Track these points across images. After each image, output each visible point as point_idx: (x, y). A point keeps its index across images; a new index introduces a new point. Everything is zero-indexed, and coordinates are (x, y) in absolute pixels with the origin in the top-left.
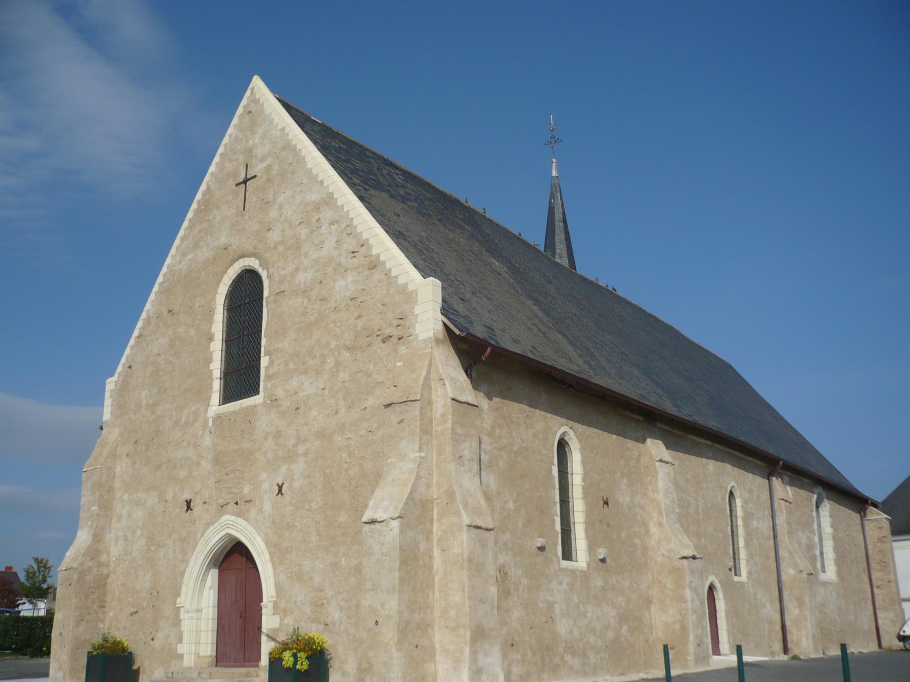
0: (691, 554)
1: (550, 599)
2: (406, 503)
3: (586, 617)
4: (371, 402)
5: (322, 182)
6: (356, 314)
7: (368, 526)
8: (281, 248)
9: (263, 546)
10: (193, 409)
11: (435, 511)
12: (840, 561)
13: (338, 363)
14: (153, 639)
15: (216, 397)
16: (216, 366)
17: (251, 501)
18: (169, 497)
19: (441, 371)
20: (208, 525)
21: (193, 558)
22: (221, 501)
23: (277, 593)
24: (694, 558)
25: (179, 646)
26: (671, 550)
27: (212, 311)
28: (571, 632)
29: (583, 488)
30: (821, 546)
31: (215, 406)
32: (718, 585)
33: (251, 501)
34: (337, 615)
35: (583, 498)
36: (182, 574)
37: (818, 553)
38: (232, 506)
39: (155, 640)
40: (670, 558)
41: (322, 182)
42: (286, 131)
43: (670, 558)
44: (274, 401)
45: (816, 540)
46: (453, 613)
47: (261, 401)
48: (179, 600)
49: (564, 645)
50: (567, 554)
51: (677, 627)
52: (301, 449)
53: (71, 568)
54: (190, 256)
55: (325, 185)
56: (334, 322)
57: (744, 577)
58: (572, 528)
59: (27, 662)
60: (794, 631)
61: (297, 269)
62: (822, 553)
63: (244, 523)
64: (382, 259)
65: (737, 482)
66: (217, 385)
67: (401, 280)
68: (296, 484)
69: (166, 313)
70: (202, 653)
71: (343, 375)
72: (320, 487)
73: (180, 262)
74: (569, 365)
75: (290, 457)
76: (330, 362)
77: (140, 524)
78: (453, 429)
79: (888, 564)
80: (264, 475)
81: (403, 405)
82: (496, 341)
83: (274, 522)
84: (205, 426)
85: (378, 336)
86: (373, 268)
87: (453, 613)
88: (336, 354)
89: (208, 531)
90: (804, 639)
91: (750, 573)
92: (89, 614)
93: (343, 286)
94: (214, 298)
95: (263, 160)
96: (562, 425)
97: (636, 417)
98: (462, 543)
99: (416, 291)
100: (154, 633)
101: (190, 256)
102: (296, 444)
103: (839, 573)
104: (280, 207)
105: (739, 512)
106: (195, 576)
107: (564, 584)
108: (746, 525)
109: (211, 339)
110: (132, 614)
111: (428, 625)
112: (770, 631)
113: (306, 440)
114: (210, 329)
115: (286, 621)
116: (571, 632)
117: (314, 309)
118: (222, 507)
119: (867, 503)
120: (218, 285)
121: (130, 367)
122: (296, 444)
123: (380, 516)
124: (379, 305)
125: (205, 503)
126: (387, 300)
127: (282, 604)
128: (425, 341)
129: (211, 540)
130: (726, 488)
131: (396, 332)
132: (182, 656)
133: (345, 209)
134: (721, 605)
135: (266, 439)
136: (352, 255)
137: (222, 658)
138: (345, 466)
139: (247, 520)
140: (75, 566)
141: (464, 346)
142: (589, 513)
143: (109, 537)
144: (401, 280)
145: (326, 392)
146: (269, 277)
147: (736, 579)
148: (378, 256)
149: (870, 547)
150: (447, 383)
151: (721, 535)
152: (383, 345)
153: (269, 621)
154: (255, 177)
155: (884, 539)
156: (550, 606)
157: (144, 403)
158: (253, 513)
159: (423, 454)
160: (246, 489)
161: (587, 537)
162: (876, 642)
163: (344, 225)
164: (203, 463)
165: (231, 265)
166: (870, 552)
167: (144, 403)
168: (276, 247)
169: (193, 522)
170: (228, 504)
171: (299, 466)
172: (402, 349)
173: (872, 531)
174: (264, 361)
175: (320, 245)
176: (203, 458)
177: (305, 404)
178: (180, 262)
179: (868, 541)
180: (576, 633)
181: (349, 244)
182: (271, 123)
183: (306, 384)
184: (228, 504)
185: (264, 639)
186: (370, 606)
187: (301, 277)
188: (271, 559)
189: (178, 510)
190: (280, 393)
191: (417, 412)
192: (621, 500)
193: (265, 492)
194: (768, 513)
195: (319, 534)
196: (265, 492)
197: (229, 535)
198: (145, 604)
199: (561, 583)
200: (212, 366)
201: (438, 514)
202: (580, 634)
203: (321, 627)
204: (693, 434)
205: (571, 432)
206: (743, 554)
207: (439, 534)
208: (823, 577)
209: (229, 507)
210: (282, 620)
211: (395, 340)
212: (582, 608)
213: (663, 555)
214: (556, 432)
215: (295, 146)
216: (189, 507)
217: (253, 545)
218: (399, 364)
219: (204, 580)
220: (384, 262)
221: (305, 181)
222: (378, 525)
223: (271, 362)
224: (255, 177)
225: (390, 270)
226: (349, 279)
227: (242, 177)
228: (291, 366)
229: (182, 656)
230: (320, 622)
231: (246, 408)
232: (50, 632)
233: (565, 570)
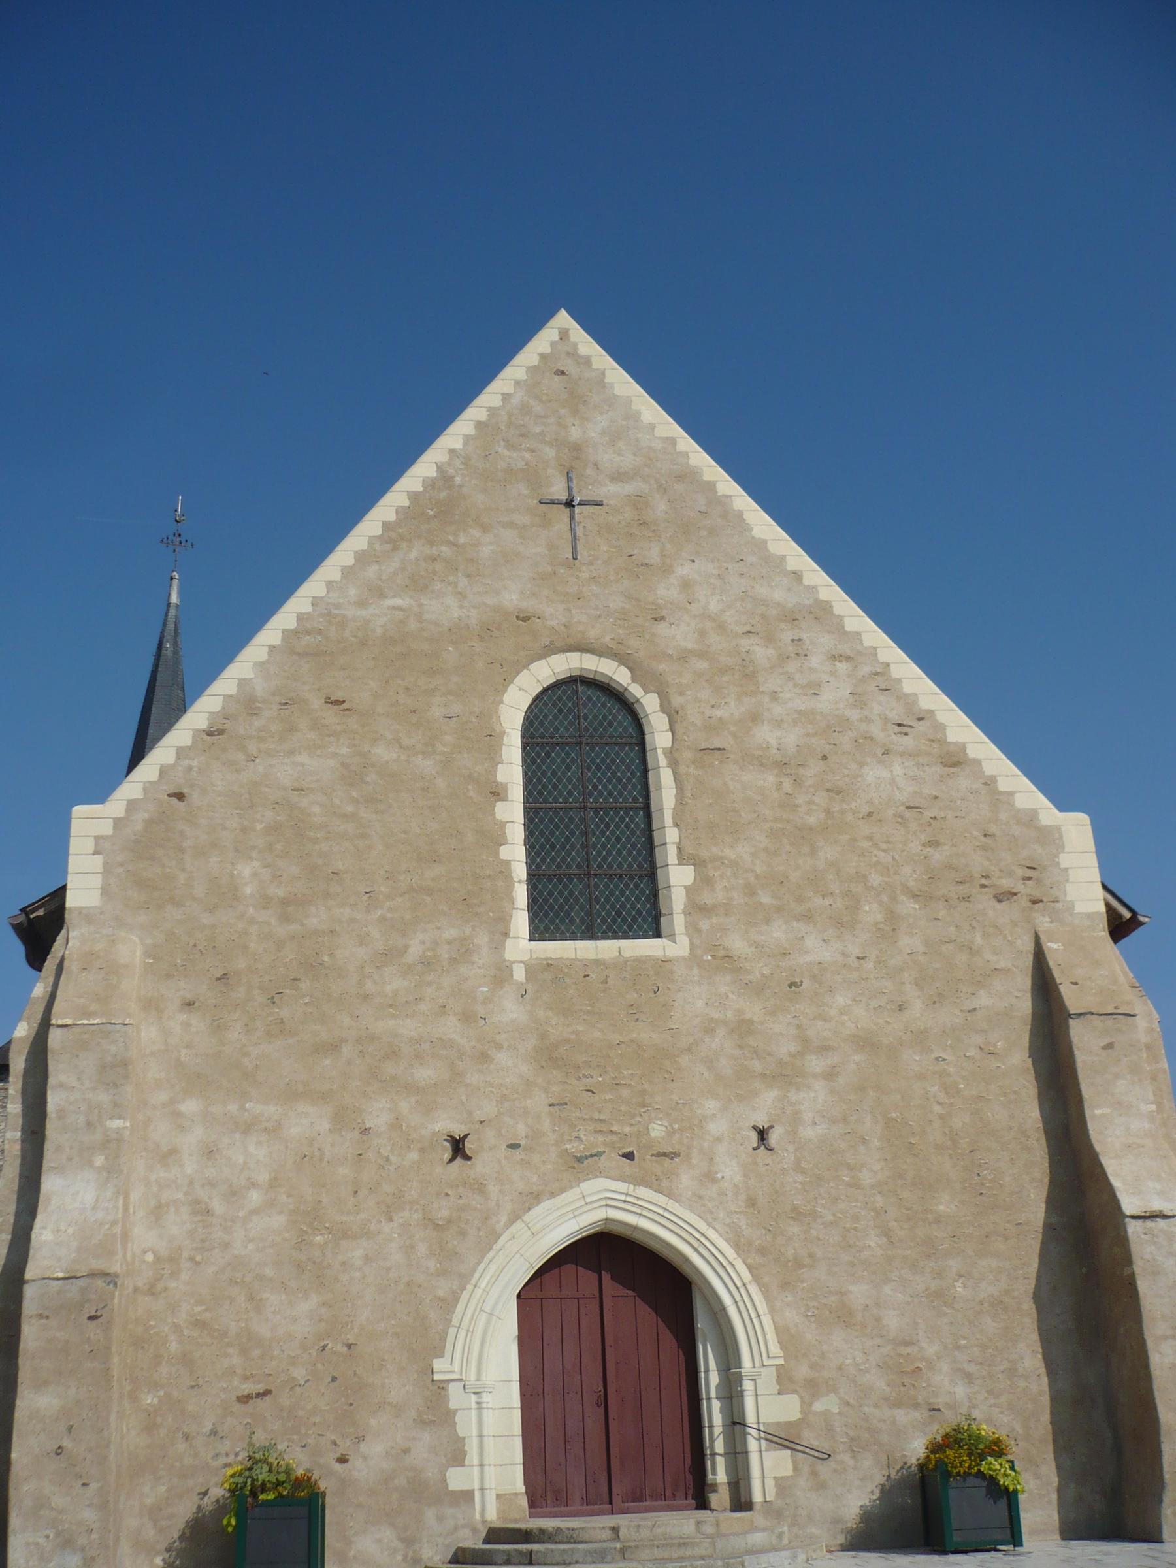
4: (983, 1000)
7: (1139, 1223)
10: (450, 933)
13: (892, 916)
15: (521, 921)
31: (520, 945)
38: (612, 1160)
39: (356, 1463)
61: (755, 718)
69: (317, 703)
71: (908, 942)
72: (876, 1143)
76: (871, 912)
77: (263, 1177)
81: (1109, 1022)
83: (752, 1202)
86: (955, 764)
88: (885, 898)
89: (537, 1211)
102: (801, 1054)
110: (245, 1399)
115: (818, 1406)
117: (811, 803)
118: (580, 1160)
120: (506, 687)
122: (801, 1054)
125: (514, 1146)
126: (993, 829)
136: (898, 729)
139: (670, 1195)
145: (869, 965)
146: (666, 708)
158: (686, 1180)
163: (866, 670)
164: (502, 1058)
169: (480, 1187)
170: (598, 1155)
171: (813, 1099)
175: (813, 689)
177: (814, 978)
178: (361, 604)
183: (810, 942)
184: (598, 1155)
187: (765, 734)
193: (719, 1139)
195: (886, 1233)
198: (299, 1373)
209: (603, 1162)
223: (704, 880)
226: (898, 770)
229: (468, 1496)
230: (916, 1406)
231: (639, 961)
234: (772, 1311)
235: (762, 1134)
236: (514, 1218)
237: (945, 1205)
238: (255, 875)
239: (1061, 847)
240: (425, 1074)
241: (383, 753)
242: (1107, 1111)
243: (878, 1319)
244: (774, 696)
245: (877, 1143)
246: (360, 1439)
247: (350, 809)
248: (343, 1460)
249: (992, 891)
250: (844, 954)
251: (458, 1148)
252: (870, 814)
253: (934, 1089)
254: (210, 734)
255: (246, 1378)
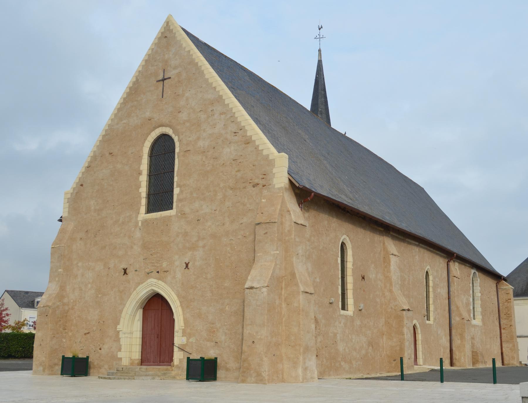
0: (407, 308)
1: (335, 331)
2: (271, 279)
3: (352, 341)
4: (245, 220)
5: (215, 88)
6: (236, 169)
8: (188, 124)
9: (175, 297)
10: (128, 214)
11: (284, 283)
12: (483, 314)
14: (100, 349)
15: (143, 209)
16: (143, 190)
17: (168, 271)
18: (111, 266)
19: (288, 206)
20: (139, 284)
21: (128, 303)
22: (147, 270)
23: (185, 324)
24: (408, 310)
25: (119, 353)
26: (396, 306)
27: (141, 157)
28: (345, 350)
29: (353, 270)
30: (474, 304)
31: (143, 215)
32: (418, 325)
33: (168, 271)
34: (223, 338)
35: (353, 276)
36: (121, 312)
37: (472, 308)
38: (155, 273)
39: (102, 350)
40: (395, 310)
41: (215, 88)
42: (191, 53)
43: (395, 310)
44: (182, 214)
45: (471, 300)
46: (293, 338)
47: (175, 214)
48: (118, 327)
49: (341, 357)
50: (343, 308)
51: (398, 348)
52: (201, 244)
53: (47, 306)
54: (125, 121)
55: (217, 90)
56: (222, 172)
57: (431, 322)
58: (346, 292)
59: (26, 361)
60: (457, 353)
61: (198, 138)
62: (474, 308)
63: (163, 284)
64: (253, 138)
65: (430, 266)
66: (144, 201)
67: (265, 153)
68: (197, 263)
69: (107, 154)
70: (133, 358)
73: (117, 124)
74: (346, 199)
75: (193, 248)
76: (220, 196)
77: (91, 281)
78: (295, 239)
79: (510, 315)
80: (177, 257)
81: (267, 225)
82: (314, 189)
83: (183, 284)
84: (136, 225)
85: (250, 183)
86: (248, 143)
87: (293, 338)
88: (224, 191)
89: (139, 288)
90: (462, 358)
91: (435, 319)
92: (58, 333)
93: (228, 152)
94: (142, 149)
95: (175, 68)
96: (344, 234)
97: (381, 229)
98: (299, 301)
99: (274, 160)
100: (101, 345)
101: (125, 121)
102: (198, 241)
103: (483, 320)
104: (187, 99)
105: (431, 284)
106: (129, 312)
107: (342, 323)
108: (434, 291)
109: (140, 173)
110: (85, 334)
111: (279, 344)
112: (444, 353)
113: (203, 239)
114: (139, 167)
115: (191, 340)
116: (345, 350)
118: (148, 273)
119: (501, 278)
120: (145, 141)
121: (82, 185)
122: (198, 241)
123: (255, 285)
124: (251, 165)
125: (136, 271)
127: (188, 331)
128: (279, 189)
129: (142, 292)
130: (425, 270)
131: (261, 182)
132: (121, 359)
133: (230, 107)
134: (419, 337)
135: (178, 236)
136: (234, 134)
137: (145, 360)
138: (229, 255)
139: (165, 282)
140: (50, 304)
141: (297, 191)
142: (355, 284)
143: (68, 288)
144: (265, 153)
145: (217, 212)
146: (180, 141)
147: (428, 322)
148: (251, 137)
149: (501, 305)
150: (291, 213)
151: (421, 297)
152: (253, 189)
153: (179, 339)
154: (170, 78)
155: (509, 301)
156: (335, 335)
157: (93, 208)
158: (169, 278)
159: (278, 252)
160: (164, 265)
161: (354, 298)
162: (501, 361)
163: (229, 116)
164: (135, 247)
165: (153, 130)
166: (501, 308)
167: (93, 208)
168: (184, 123)
169: (129, 282)
170: (152, 272)
171: (199, 253)
172: (265, 192)
173: (503, 296)
174: (176, 191)
175: (214, 126)
176: (135, 244)
178: (117, 124)
179: (500, 301)
180: (347, 350)
181: (233, 128)
182: (181, 46)
184: (152, 272)
185: (176, 349)
186: (249, 333)
187: (201, 143)
188: (181, 305)
189: (117, 274)
190: (187, 210)
191: (276, 229)
192: (371, 277)
193: (177, 267)
194: (446, 284)
196: (177, 267)
197: (153, 290)
198: (95, 328)
199: (340, 323)
200: (140, 190)
201: (285, 285)
202: (349, 351)
203: (213, 344)
204: (409, 238)
205: (347, 238)
206: (432, 308)
207: (286, 295)
208: (474, 322)
209: (152, 274)
210: (188, 340)
211: (261, 186)
212: (350, 337)
213: (392, 308)
214: (340, 239)
215: (197, 63)
216: (125, 273)
217: (169, 297)
218: (263, 200)
219: (135, 316)
220: (254, 141)
221: (204, 86)
222: (254, 290)
223: (181, 192)
224: (170, 78)
225: (258, 146)
226: (232, 148)
227: (161, 77)
228: (195, 195)
229: (121, 359)
230: (212, 341)
231: (165, 217)
232: (33, 343)
233: (343, 315)
234: (183, 314)
235: (187, 265)
236: (135, 289)
237: (227, 284)
238: (94, 204)
239: (273, 166)
240: (121, 253)
241: (119, 166)
242: (261, 254)
243: (207, 317)
244: (204, 131)
245: (213, 266)
246: (104, 344)
247: (111, 183)
248: (100, 349)
249: (252, 184)
250: (212, 210)
251: (125, 272)
252: (223, 164)
253: (228, 249)
254: (88, 167)
255: (86, 329)
